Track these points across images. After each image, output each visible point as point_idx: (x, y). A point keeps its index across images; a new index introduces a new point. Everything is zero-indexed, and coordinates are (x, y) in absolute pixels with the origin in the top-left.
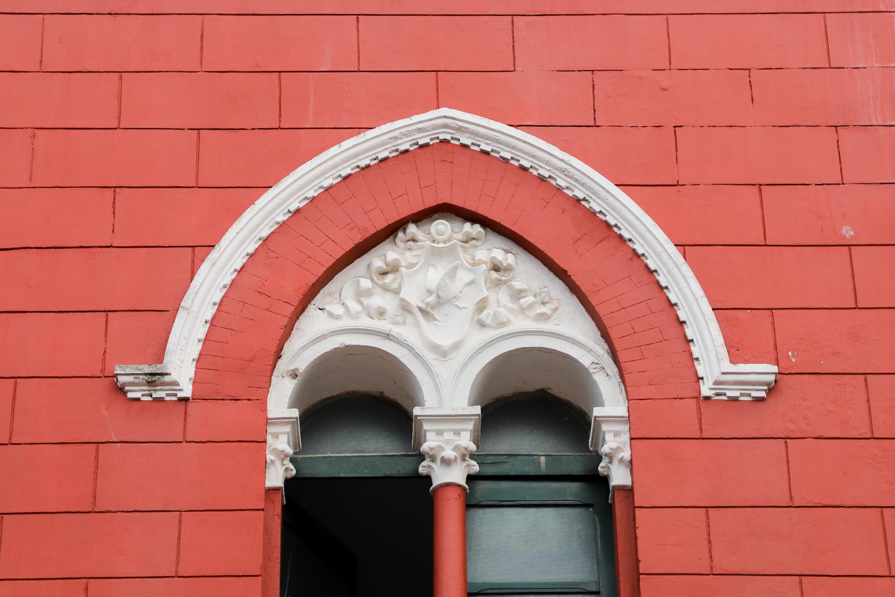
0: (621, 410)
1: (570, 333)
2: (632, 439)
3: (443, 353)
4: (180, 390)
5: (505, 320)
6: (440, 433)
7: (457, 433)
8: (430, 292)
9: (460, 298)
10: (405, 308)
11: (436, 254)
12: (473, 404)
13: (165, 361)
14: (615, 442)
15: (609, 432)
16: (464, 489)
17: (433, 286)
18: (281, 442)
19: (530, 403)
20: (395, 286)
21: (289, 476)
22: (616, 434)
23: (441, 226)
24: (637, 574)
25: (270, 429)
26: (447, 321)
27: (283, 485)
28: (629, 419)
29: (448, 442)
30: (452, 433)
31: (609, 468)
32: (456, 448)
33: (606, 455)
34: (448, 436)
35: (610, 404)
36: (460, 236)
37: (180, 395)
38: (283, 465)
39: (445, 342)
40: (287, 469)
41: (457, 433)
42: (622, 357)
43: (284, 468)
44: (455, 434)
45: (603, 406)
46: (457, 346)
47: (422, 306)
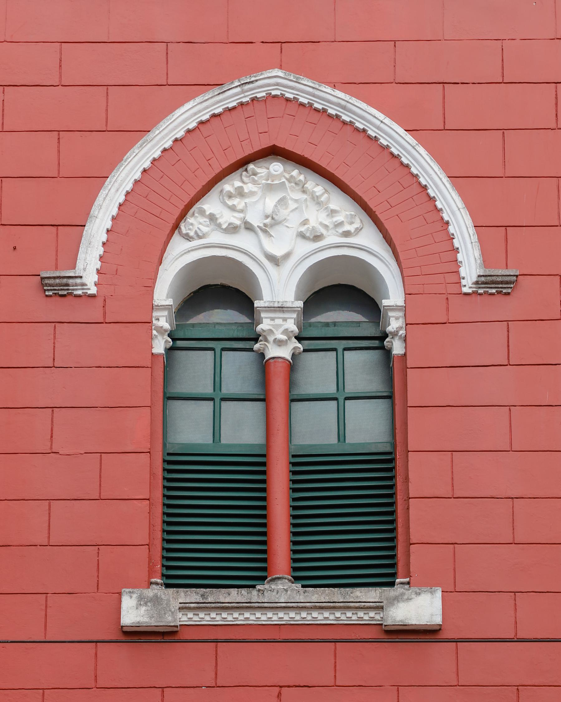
0: (400, 302)
1: (369, 246)
2: (407, 325)
3: (275, 260)
4: (89, 289)
5: (319, 234)
6: (273, 319)
7: (285, 320)
8: (267, 217)
9: (288, 220)
10: (249, 227)
11: (270, 188)
12: (297, 299)
13: (77, 268)
14: (395, 324)
15: (393, 317)
16: (290, 362)
17: (269, 211)
18: (163, 321)
19: (339, 292)
20: (240, 206)
21: (168, 347)
22: (397, 318)
23: (276, 167)
24: (406, 407)
25: (155, 314)
26: (280, 232)
27: (164, 352)
28: (404, 309)
29: (278, 326)
30: (281, 320)
31: (392, 342)
32: (285, 332)
33: (391, 333)
34: (279, 322)
35: (393, 296)
36: (287, 176)
37: (89, 292)
38: (163, 339)
39: (278, 252)
40: (166, 341)
41: (285, 320)
42: (401, 256)
43: (164, 340)
44: (283, 321)
45: (389, 299)
46: (287, 256)
47: (261, 225)
